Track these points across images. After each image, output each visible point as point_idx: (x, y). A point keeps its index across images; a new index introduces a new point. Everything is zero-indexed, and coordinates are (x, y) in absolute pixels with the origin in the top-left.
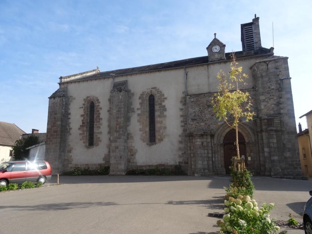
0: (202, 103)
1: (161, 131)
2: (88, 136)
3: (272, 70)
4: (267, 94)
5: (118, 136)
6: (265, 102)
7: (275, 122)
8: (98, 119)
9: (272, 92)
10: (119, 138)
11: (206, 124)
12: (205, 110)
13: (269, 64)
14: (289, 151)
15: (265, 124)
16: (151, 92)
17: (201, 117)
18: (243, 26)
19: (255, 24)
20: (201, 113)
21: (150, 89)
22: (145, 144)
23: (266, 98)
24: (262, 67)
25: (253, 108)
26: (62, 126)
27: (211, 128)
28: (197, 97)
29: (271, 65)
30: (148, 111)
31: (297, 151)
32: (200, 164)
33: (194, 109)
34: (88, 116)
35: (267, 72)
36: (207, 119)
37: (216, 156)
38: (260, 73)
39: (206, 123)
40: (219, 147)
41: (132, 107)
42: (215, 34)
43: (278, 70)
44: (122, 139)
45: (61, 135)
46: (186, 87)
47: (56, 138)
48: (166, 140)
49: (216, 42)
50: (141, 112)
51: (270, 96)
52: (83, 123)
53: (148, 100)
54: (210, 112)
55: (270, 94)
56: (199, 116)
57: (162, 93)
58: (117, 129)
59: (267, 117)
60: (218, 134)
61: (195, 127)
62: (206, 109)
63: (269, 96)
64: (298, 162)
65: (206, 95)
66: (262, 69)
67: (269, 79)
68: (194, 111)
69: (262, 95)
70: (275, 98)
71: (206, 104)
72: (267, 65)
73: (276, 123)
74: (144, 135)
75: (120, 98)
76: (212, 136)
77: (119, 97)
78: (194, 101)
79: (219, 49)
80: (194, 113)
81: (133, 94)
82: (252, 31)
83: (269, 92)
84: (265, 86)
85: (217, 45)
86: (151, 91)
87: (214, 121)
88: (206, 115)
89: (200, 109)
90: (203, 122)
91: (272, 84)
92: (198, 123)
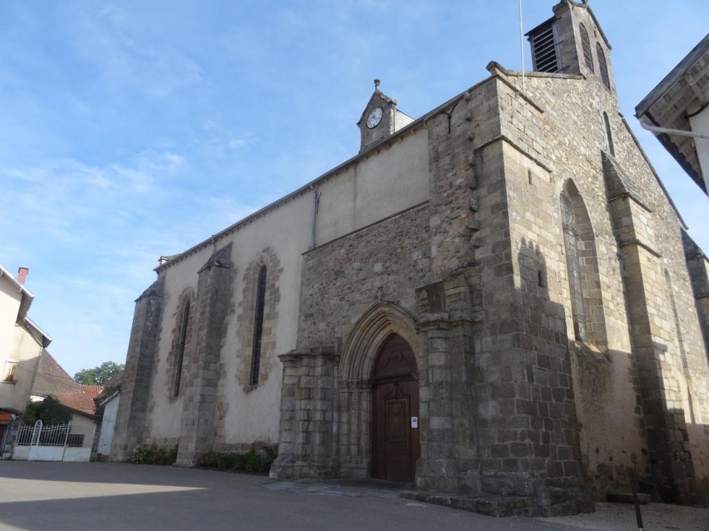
1: (268, 355)
6: (440, 232)
9: (457, 198)
10: (196, 377)
14: (493, 397)
15: (424, 305)
22: (241, 388)
23: (443, 222)
24: (437, 129)
27: (336, 336)
30: (255, 308)
32: (285, 442)
35: (448, 139)
36: (330, 309)
37: (345, 419)
39: (329, 323)
40: (355, 391)
43: (473, 124)
50: (244, 311)
51: (452, 209)
52: (173, 347)
53: (257, 280)
60: (353, 353)
61: (309, 337)
62: (331, 284)
63: (449, 212)
64: (518, 441)
65: (335, 244)
68: (310, 292)
69: (435, 213)
70: (464, 216)
71: (333, 270)
72: (450, 118)
74: (242, 366)
76: (331, 357)
78: (313, 267)
80: (311, 297)
81: (236, 272)
87: (344, 314)
89: (322, 284)
90: (324, 320)
92: (315, 324)
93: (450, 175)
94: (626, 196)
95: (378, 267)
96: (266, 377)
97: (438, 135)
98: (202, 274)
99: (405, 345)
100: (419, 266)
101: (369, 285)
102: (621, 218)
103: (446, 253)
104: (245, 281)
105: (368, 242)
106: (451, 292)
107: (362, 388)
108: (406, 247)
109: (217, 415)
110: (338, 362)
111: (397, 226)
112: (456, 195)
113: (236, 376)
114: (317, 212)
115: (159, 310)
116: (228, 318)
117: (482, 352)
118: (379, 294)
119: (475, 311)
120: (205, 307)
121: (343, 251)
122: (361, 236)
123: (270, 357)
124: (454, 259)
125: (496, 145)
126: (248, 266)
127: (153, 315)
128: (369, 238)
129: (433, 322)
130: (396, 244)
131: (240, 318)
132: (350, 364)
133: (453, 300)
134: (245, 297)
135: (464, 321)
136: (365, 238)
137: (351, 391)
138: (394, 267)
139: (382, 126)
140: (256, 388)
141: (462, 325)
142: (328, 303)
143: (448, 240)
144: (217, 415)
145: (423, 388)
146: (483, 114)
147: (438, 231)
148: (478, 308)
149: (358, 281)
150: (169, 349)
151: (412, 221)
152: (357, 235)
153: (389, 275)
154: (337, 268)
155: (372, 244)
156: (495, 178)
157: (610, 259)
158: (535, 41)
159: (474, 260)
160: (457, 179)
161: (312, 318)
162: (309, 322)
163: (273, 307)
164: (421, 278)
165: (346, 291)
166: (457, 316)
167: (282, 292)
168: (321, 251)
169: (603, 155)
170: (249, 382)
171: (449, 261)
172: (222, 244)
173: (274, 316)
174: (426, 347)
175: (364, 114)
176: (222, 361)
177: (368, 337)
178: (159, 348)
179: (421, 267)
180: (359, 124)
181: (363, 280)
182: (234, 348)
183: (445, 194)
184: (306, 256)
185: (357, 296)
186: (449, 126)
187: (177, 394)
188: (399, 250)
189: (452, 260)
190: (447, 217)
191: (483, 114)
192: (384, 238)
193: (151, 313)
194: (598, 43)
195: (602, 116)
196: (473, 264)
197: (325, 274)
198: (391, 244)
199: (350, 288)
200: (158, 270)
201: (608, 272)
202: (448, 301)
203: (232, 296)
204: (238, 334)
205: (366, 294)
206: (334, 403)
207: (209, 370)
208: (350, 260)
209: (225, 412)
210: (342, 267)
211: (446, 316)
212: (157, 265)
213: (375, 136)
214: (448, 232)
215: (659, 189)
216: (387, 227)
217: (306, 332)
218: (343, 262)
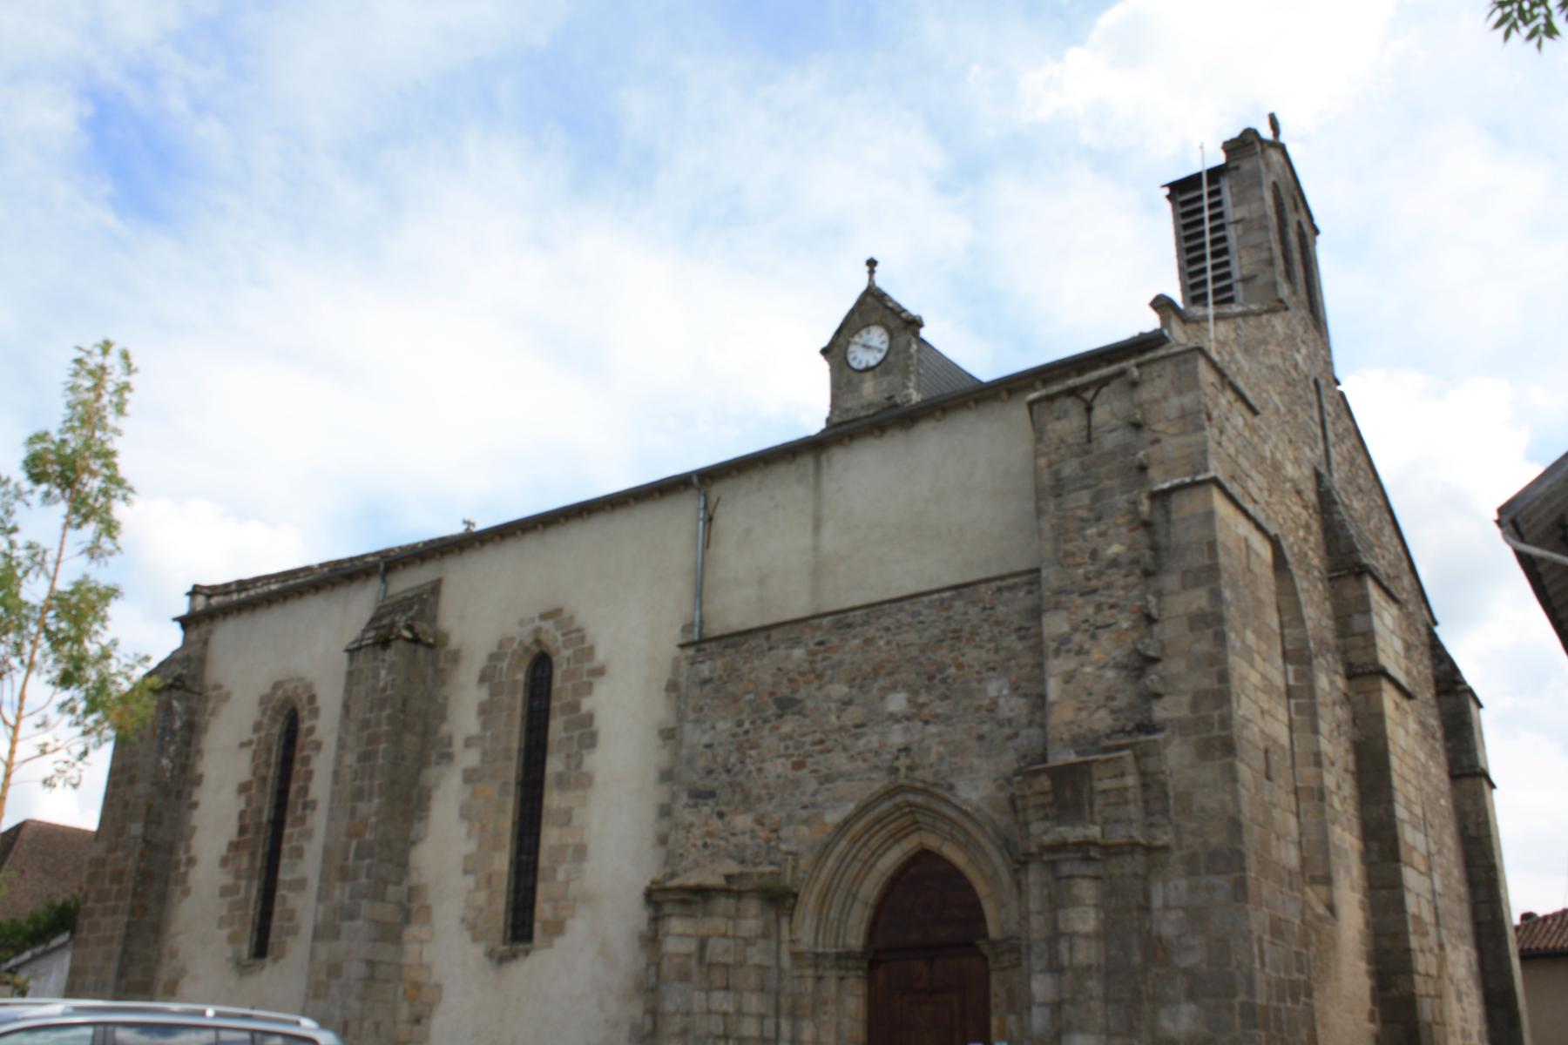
0: (751, 687)
1: (561, 876)
3: (1114, 435)
4: (1080, 601)
5: (347, 901)
6: (1069, 651)
7: (1100, 786)
8: (300, 807)
9: (1109, 586)
10: (352, 916)
11: (759, 821)
12: (766, 732)
13: (1096, 403)
14: (1191, 995)
15: (1043, 806)
17: (741, 778)
19: (1237, 168)
20: (740, 749)
21: (532, 620)
22: (479, 950)
23: (1075, 629)
25: (1022, 701)
26: (149, 845)
27: (783, 847)
28: (731, 651)
29: (1107, 407)
31: (1241, 997)
33: (707, 726)
34: (269, 790)
35: (1087, 452)
36: (766, 786)
38: (1050, 465)
39: (763, 816)
41: (445, 729)
42: (872, 263)
43: (1147, 436)
44: (359, 923)
45: (135, 894)
46: (699, 594)
47: (114, 911)
48: (578, 927)
49: (874, 307)
50: (483, 761)
51: (1099, 608)
52: (242, 830)
54: (790, 743)
55: (1097, 598)
56: (728, 771)
57: (582, 639)
58: (346, 858)
59: (1077, 753)
61: (705, 845)
62: (768, 726)
63: (1090, 610)
65: (775, 634)
66: (1062, 441)
68: (706, 739)
69: (1056, 608)
70: (1125, 625)
71: (772, 694)
72: (1089, 409)
73: (1104, 792)
74: (481, 898)
75: (381, 684)
76: (779, 899)
77: (376, 676)
79: (885, 347)
80: (709, 751)
81: (455, 657)
83: (1094, 583)
84: (1070, 547)
85: (876, 323)
87: (806, 799)
88: (767, 765)
89: (740, 724)
90: (748, 810)
91: (1111, 532)
92: (721, 815)
93: (1091, 531)
94: (1361, 572)
95: (897, 702)
96: (557, 927)
97: (1062, 441)
98: (361, 656)
99: (955, 879)
100: (1004, 712)
101: (872, 739)
102: (1350, 616)
103: (1084, 698)
104: (486, 685)
105: (868, 642)
106: (1107, 784)
107: (847, 969)
108: (971, 666)
109: (404, 1011)
110: (793, 908)
111: (945, 614)
112: (1105, 578)
113: (463, 920)
114: (707, 544)
115: (193, 729)
116: (432, 773)
117: (1166, 907)
118: (903, 762)
119: (1151, 825)
120: (373, 740)
121: (798, 653)
122: (850, 626)
123: (567, 882)
124: (1102, 713)
125: (1199, 493)
126: (494, 649)
127: (178, 739)
128: (871, 632)
129: (1074, 844)
130: (944, 655)
131: (469, 777)
132: (820, 913)
133: (1112, 800)
134: (485, 726)
135: (1137, 844)
136: (859, 630)
137: (821, 972)
138: (941, 708)
139: (887, 372)
140: (527, 953)
141: (1132, 852)
142: (759, 770)
143: (1088, 669)
144: (404, 1011)
145: (1040, 977)
146: (1168, 420)
147: (1064, 648)
148: (1158, 818)
149: (841, 729)
150: (231, 831)
151: (984, 609)
152: (839, 621)
153: (927, 722)
154: (784, 690)
155: (879, 649)
156: (1197, 560)
157: (1334, 703)
158: (1184, 204)
159: (1150, 720)
160: (1110, 544)
161: (711, 802)
162: (706, 810)
163: (575, 760)
164: (1010, 738)
165: (808, 747)
166: (1119, 835)
167: (603, 725)
168: (734, 645)
169: (1318, 476)
170: (499, 935)
171: (1091, 715)
172: (405, 582)
173: (580, 780)
174: (1046, 892)
175: (839, 332)
176: (414, 879)
177: (863, 855)
178: (194, 829)
179: (1008, 714)
180: (825, 352)
181: (857, 726)
182: (454, 846)
183: (1081, 571)
184: (690, 652)
185: (839, 761)
186: (1089, 427)
187: (261, 948)
188: (952, 671)
189: (1097, 716)
190: (1086, 621)
191: (1168, 420)
192: (911, 637)
193: (173, 733)
194: (1299, 224)
195: (1312, 386)
196: (1148, 727)
197: (750, 702)
198: (929, 654)
199: (821, 742)
200: (186, 622)
201: (1331, 732)
202: (1099, 801)
203: (443, 717)
204: (466, 814)
205: (865, 760)
206: (782, 999)
207: (383, 900)
208: (820, 677)
209: (431, 1006)
210: (794, 692)
211: (1094, 831)
212: (183, 608)
213: (870, 390)
214: (1087, 653)
215: (1396, 541)
216: (919, 614)
217: (697, 832)
218: (800, 679)
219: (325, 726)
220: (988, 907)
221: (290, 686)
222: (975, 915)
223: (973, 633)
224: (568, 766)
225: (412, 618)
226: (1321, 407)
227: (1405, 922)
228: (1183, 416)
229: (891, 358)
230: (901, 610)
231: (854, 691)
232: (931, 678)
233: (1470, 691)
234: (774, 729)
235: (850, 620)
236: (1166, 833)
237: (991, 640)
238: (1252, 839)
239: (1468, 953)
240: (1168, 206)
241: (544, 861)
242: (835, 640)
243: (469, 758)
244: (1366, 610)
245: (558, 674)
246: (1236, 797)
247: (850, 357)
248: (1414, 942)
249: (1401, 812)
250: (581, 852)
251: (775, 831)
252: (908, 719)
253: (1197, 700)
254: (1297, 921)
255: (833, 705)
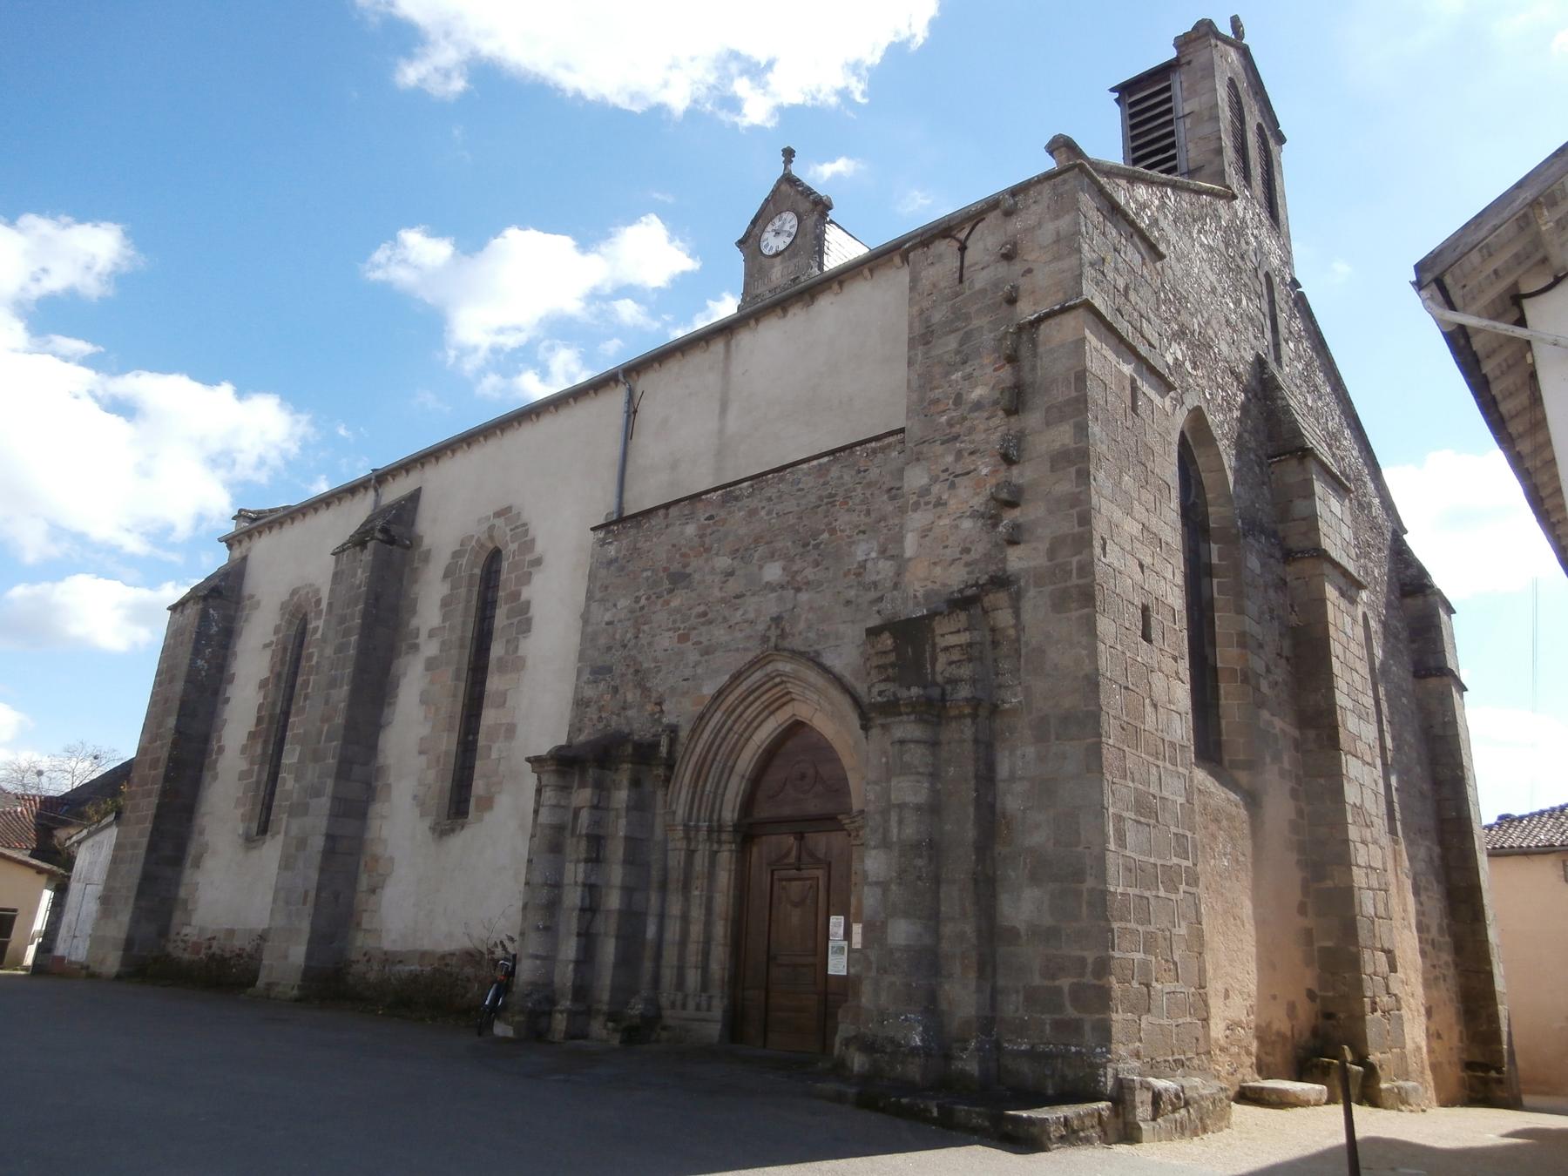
1: (494, 755)
2: (262, 787)
6: (927, 503)
7: (942, 642)
9: (972, 430)
14: (1034, 879)
16: (491, 537)
18: (1125, 91)
19: (1189, 63)
23: (935, 480)
24: (932, 271)
31: (1090, 882)
35: (957, 295)
36: (655, 660)
41: (415, 622)
42: (789, 154)
43: (1018, 267)
48: (503, 802)
51: (959, 455)
63: (950, 459)
64: (1089, 979)
65: (673, 511)
67: (967, 337)
68: (608, 617)
69: (918, 460)
70: (985, 471)
71: (665, 569)
72: (963, 249)
73: (946, 649)
74: (431, 775)
77: (355, 575)
78: (616, 560)
79: (794, 231)
81: (426, 557)
82: (1170, 111)
83: (956, 429)
86: (492, 528)
87: (688, 673)
89: (637, 599)
93: (957, 376)
96: (487, 803)
105: (753, 513)
112: (967, 424)
113: (415, 797)
120: (347, 633)
121: (691, 530)
128: (754, 503)
131: (431, 665)
132: (695, 787)
133: (955, 658)
134: (445, 618)
138: (810, 573)
145: (874, 852)
149: (723, 600)
151: (859, 472)
153: (798, 590)
154: (675, 567)
156: (1062, 393)
157: (1266, 587)
158: (1132, 105)
159: (1005, 571)
163: (513, 645)
167: (536, 612)
173: (515, 664)
175: (754, 222)
179: (874, 578)
181: (737, 597)
184: (601, 534)
185: (719, 634)
188: (826, 536)
197: (647, 578)
199: (705, 614)
200: (230, 541)
208: (708, 550)
213: (778, 274)
219: (318, 624)
220: (853, 781)
221: (303, 592)
222: (839, 789)
223: (847, 498)
224: (507, 652)
225: (388, 522)
226: (1272, 302)
227: (1344, 811)
228: (1057, 241)
229: (798, 241)
230: (782, 480)
231: (735, 563)
232: (806, 545)
233: (1439, 593)
234: (667, 603)
235: (738, 493)
236: (1015, 695)
237: (863, 502)
238: (1112, 702)
239: (1429, 849)
240: (1118, 109)
241: (482, 741)
242: (723, 514)
243: (430, 649)
244: (1310, 495)
245: (505, 565)
246: (1093, 654)
247: (763, 245)
248: (1353, 833)
249: (1341, 699)
250: (511, 730)
251: (660, 704)
252: (782, 587)
253: (1056, 545)
254: (1181, 800)
255: (717, 579)
